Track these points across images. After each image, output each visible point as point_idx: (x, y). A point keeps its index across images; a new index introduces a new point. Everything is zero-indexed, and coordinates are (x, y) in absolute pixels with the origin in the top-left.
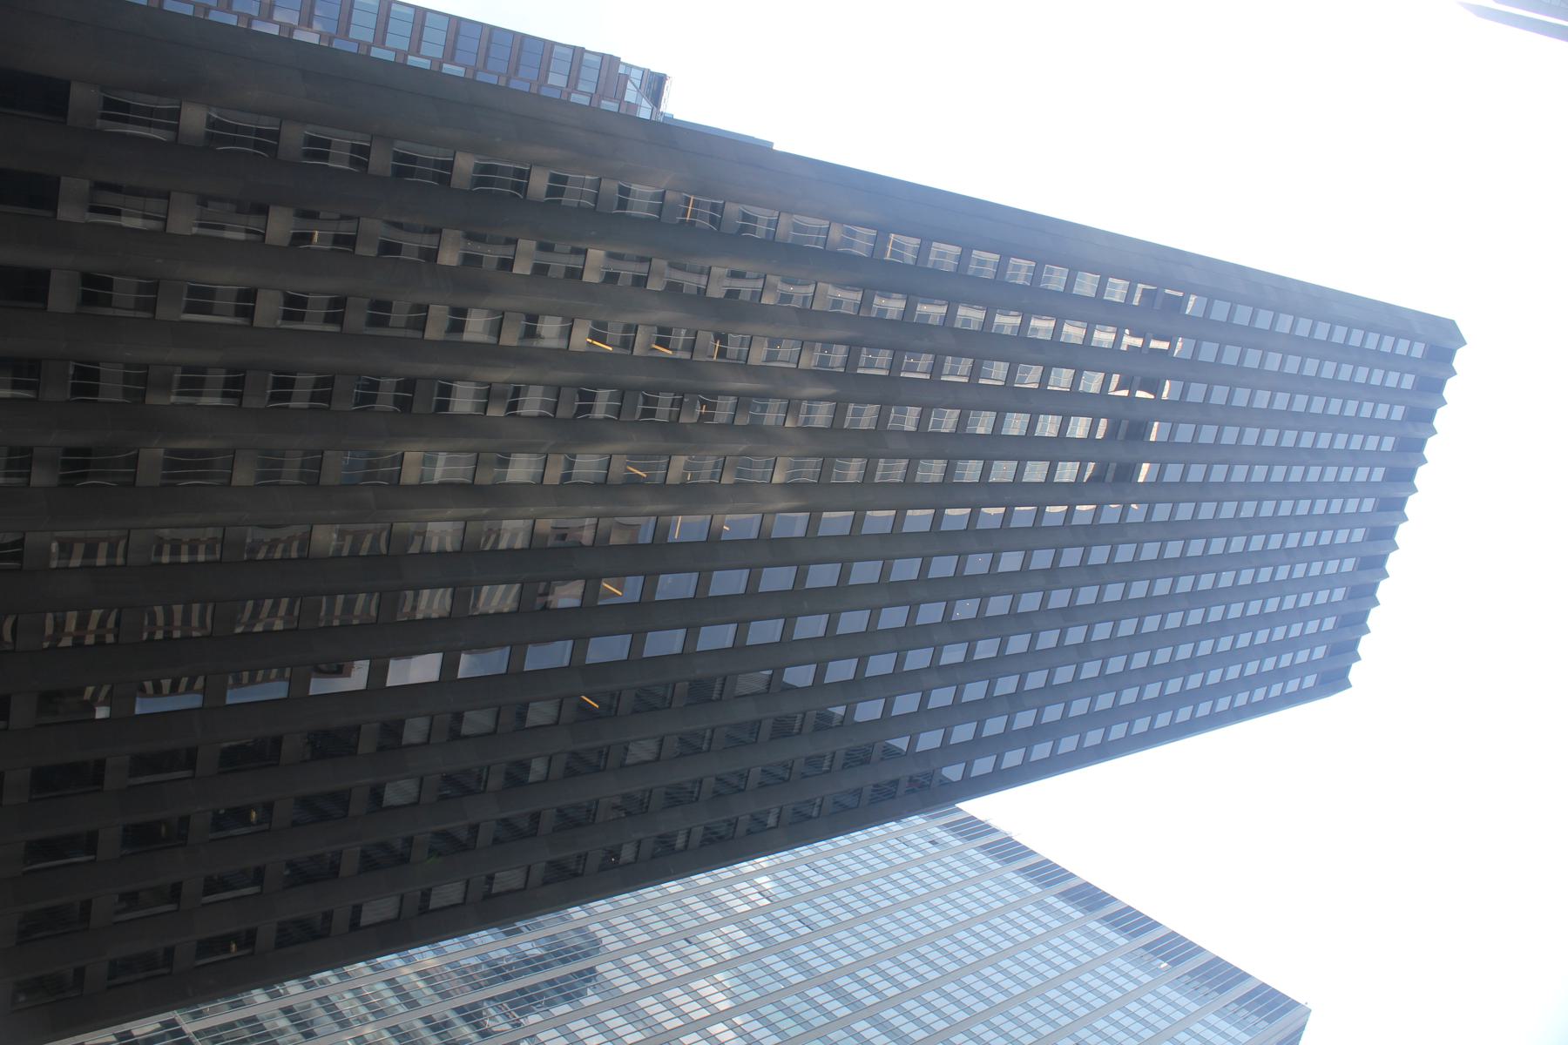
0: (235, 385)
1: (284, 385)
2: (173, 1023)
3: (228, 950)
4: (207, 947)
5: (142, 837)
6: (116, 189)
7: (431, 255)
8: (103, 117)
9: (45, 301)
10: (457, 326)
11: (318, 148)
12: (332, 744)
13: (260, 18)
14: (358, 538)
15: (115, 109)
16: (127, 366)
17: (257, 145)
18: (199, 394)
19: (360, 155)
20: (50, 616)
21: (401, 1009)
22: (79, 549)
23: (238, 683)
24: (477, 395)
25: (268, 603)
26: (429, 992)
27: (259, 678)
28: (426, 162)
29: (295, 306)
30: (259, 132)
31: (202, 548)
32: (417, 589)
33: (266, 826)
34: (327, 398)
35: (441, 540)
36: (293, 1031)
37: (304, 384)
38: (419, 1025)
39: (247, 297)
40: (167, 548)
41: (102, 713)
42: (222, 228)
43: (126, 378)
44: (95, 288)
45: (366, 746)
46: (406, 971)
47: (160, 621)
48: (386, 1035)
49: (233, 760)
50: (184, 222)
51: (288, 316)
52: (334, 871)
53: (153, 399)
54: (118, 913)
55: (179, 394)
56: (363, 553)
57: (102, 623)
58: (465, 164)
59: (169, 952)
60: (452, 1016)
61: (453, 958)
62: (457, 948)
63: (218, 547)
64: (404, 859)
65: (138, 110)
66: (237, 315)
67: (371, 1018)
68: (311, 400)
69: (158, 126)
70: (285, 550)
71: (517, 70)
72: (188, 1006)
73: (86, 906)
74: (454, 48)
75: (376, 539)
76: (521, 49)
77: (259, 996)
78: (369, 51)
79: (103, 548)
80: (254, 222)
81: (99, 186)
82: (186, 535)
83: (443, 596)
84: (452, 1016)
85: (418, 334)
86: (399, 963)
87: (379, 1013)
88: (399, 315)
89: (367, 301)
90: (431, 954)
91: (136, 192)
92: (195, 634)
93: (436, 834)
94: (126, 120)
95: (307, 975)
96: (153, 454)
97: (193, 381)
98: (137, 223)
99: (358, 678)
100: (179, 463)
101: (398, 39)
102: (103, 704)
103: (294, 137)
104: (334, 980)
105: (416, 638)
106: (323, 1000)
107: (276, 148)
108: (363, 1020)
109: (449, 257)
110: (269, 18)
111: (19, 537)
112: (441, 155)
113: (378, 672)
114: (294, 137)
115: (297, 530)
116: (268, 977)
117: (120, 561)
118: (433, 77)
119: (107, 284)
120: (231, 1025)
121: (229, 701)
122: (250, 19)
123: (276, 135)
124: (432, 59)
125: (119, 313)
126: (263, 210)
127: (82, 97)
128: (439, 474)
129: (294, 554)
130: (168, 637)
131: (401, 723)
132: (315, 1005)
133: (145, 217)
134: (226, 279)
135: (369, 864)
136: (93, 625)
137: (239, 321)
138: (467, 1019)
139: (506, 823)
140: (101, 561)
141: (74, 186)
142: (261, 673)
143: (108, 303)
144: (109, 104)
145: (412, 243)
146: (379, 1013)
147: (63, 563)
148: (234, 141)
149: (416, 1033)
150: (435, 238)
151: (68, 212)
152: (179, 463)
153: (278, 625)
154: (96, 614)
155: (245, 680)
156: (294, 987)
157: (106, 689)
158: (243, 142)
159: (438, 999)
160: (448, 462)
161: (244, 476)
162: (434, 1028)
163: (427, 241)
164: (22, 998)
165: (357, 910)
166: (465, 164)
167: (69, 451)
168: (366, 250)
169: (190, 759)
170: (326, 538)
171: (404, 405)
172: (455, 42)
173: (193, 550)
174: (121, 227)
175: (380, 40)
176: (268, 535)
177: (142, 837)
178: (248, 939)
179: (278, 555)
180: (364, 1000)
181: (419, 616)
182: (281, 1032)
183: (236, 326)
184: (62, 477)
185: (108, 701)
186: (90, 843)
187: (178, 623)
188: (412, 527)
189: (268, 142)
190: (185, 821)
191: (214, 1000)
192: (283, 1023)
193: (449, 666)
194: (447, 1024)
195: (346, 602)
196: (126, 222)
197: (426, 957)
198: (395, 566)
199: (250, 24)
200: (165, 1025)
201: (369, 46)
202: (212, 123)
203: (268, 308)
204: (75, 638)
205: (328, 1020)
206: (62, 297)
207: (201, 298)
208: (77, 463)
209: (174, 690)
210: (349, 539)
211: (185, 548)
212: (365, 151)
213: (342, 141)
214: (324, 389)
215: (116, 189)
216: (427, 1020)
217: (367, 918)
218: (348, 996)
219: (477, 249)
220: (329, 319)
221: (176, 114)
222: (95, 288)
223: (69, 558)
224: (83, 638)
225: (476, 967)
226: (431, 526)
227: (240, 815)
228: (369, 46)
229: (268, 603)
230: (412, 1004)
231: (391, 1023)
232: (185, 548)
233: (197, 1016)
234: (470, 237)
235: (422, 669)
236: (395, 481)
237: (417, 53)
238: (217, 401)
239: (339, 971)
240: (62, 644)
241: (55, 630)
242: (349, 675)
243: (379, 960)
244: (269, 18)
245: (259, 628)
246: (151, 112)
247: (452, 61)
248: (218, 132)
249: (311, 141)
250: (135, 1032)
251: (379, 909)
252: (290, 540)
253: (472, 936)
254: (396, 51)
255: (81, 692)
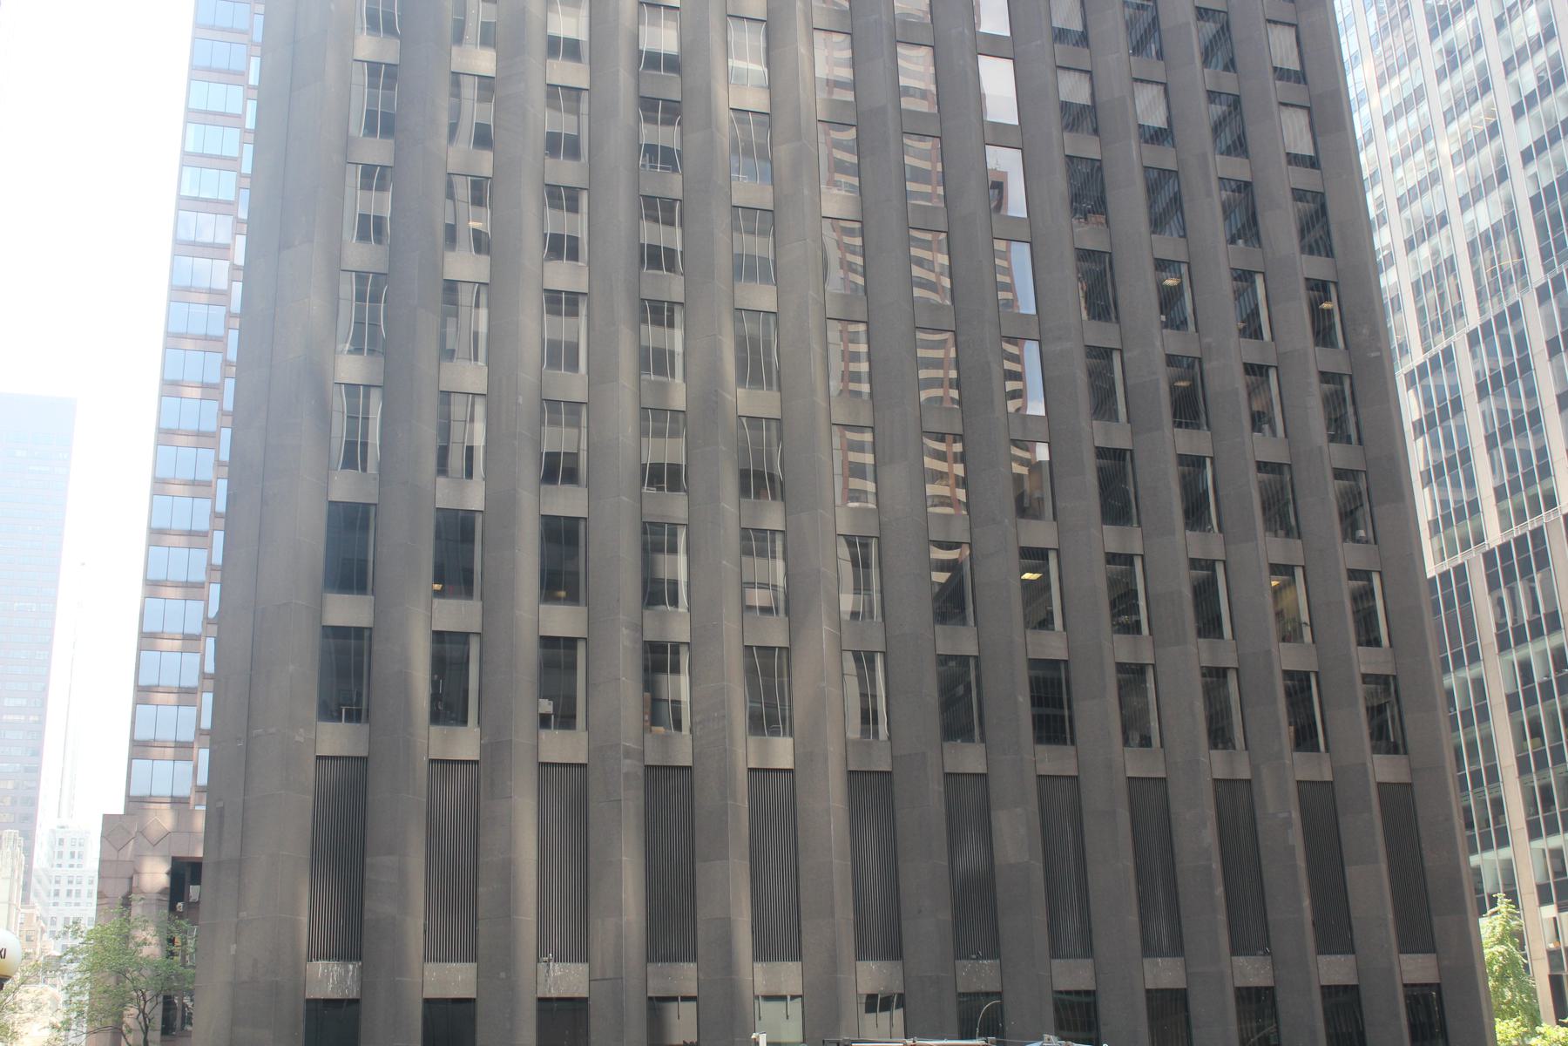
0: (658, 312)
1: (656, 257)
2: (1410, 378)
3: (1330, 312)
4: (1323, 333)
6: (443, 454)
7: (487, 85)
8: (364, 469)
9: (577, 519)
10: (571, 49)
11: (370, 228)
12: (1088, 192)
13: (227, 304)
14: (839, 167)
15: (354, 456)
16: (643, 432)
17: (375, 299)
18: (672, 353)
19: (373, 177)
21: (1424, 107)
22: (855, 483)
23: (1011, 303)
24: (654, 23)
25: (917, 271)
26: (1405, 73)
27: (1007, 280)
28: (372, 99)
29: (561, 247)
30: (360, 297)
32: (900, 92)
33: (1184, 268)
34: (669, 205)
35: (838, 64)
36: (1435, 239)
37: (654, 234)
38: (1446, 85)
39: (560, 302)
40: (852, 386)
41: (1042, 453)
42: (476, 334)
43: (659, 434)
44: (557, 470)
45: (1089, 148)
46: (1375, 102)
47: (938, 392)
48: (1454, 127)
49: (1101, 299)
50: (471, 376)
51: (574, 255)
52: (1245, 187)
53: (678, 400)
55: (673, 376)
56: (855, 159)
57: (941, 456)
58: (367, 47)
59: (1325, 377)
60: (1440, 44)
61: (1366, 43)
62: (1353, 39)
63: (852, 328)
64: (1236, 103)
65: (351, 431)
66: (576, 314)
67: (1431, 145)
68: (673, 224)
70: (854, 253)
71: (235, 73)
72: (1392, 360)
73: (1262, 466)
74: (228, 72)
75: (838, 145)
76: (212, 28)
77: (1388, 280)
78: (246, 176)
79: (854, 457)
80: (466, 296)
81: (442, 468)
82: (837, 365)
83: (907, 59)
84: (1440, 44)
85: (585, 95)
86: (1365, 110)
87: (1425, 136)
88: (564, 124)
89: (549, 161)
90: (1358, 72)
91: (445, 429)
92: (953, 354)
93: (1206, 62)
95: (1369, 223)
96: (747, 401)
97: (656, 361)
98: (479, 428)
99: (1005, 161)
100: (754, 368)
101: (217, 229)
102: (1033, 452)
103: (360, 255)
104: (1378, 190)
105: (957, 88)
106: (1402, 203)
107: (377, 274)
108: (1433, 156)
109: (484, 62)
110: (226, 294)
111: (842, 541)
112: (361, 77)
113: (1001, 135)
114: (360, 255)
115: (830, 237)
116: (1366, 268)
118: (265, 96)
119: (552, 458)
120: (1421, 311)
121: (1033, 311)
122: (229, 315)
123: (361, 277)
124: (246, 98)
125: (584, 445)
126: (451, 287)
127: (345, 487)
128: (758, 69)
129: (858, 241)
130: (957, 384)
131: (1065, 106)
132: (1407, 213)
133: (472, 420)
134: (532, 327)
135: (1239, 147)
137: (583, 310)
138: (1446, 23)
139: (1207, 56)
140: (868, 459)
141: (447, 494)
142: (1000, 278)
144: (349, 462)
145: (474, 112)
146: (1425, 136)
147: (871, 498)
148: (374, 325)
149: (1455, 91)
150: (465, 80)
151: (474, 498)
152: (754, 368)
154: (930, 463)
155: (1009, 296)
156: (1382, 239)
157: (1016, 451)
159: (1416, 62)
160: (741, 57)
161: (763, 297)
162: (1453, 66)
163: (470, 90)
164: (1362, 533)
165: (1294, 159)
166: (367, 47)
167: (744, 491)
168: (485, 163)
169: (1100, 355)
170: (836, 201)
171: (672, 112)
172: (219, 71)
173: (855, 357)
174: (486, 447)
175: (231, 163)
176: (836, 274)
178: (1319, 288)
179: (859, 260)
180: (1406, 155)
181: (933, 88)
182: (1435, 253)
183: (588, 316)
184: (774, 498)
186: (1192, 464)
187: (940, 373)
188: (822, 95)
189: (371, 288)
190: (1171, 360)
191: (1387, 331)
192: (1424, 251)
193: (994, 47)
194: (1450, 51)
195: (916, 181)
196: (479, 441)
197: (1359, 78)
198: (869, 119)
200: (1411, 383)
201: (241, 176)
203: (563, 276)
205: (1427, 197)
206: (567, 502)
207: (560, 355)
210: (838, 177)
211: (853, 367)
212: (368, 171)
213: (359, 201)
214: (658, 209)
215: (443, 454)
216: (1441, 75)
217: (1305, 148)
218: (1399, 173)
219: (473, 30)
220: (574, 208)
221: (352, 388)
222: (557, 470)
223: (865, 492)
224: (957, 476)
225: (1380, 14)
226: (822, 71)
227: (1169, 300)
228: (241, 176)
229: (917, 271)
230: (1419, 95)
231: (1439, 120)
232: (853, 367)
233: (1404, 349)
234: (459, 38)
235: (998, 83)
236: (767, 119)
237: (241, 117)
238: (678, 334)
239: (1367, 185)
240: (964, 499)
242: (1005, 174)
243: (1359, 135)
244: (226, 294)
245: (946, 282)
246: (352, 418)
247: (243, 74)
248: (366, 340)
249: (363, 236)
250: (1416, 417)
251: (1295, 133)
252: (840, 244)
253: (1339, 19)
254: (242, 143)
255: (1018, 478)
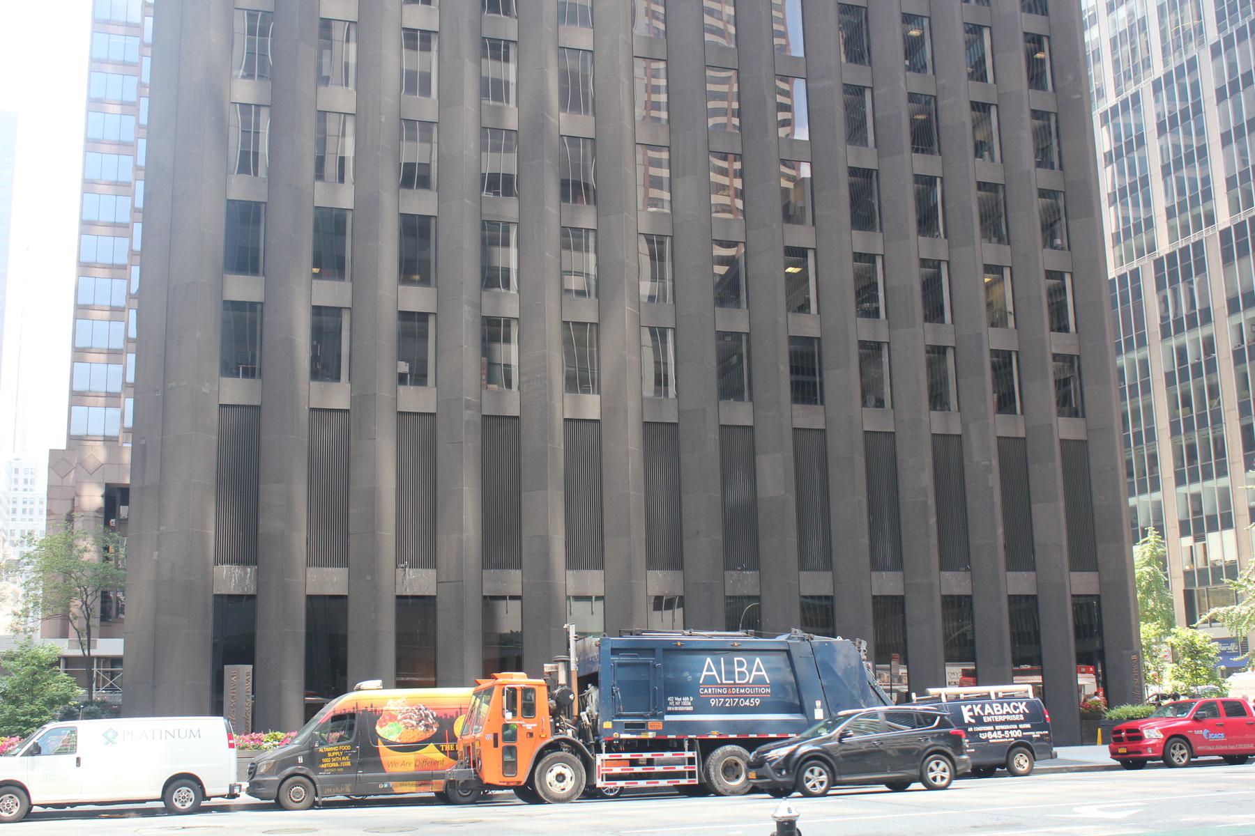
0: (496, 49)
3: (1042, 61)
4: (1036, 79)
5: (924, 137)
8: (256, 174)
9: (429, 217)
13: (141, 36)
17: (264, 33)
18: (507, 83)
20: (714, 215)
22: (654, 193)
23: (784, 48)
25: (708, 20)
27: (781, 28)
30: (251, 32)
31: (654, 82)
33: (926, 22)
39: (416, 39)
40: (654, 113)
41: (805, 171)
42: (347, 65)
44: (413, 177)
50: (342, 99)
53: (512, 122)
54: (992, 159)
55: (508, 101)
57: (723, 172)
59: (1036, 114)
63: (654, 65)
65: (245, 143)
66: (429, 50)
69: (257, 125)
72: (1090, 102)
77: (1091, 36)
79: (654, 171)
80: (338, 33)
81: (320, 174)
82: (641, 97)
91: (322, 143)
92: (735, 89)
94: (256, 154)
96: (568, 123)
97: (494, 90)
98: (350, 142)
100: (573, 97)
111: (642, 239)
117: (665, 155)
119: (410, 167)
120: (1116, 63)
121: (801, 54)
123: (252, 15)
125: (435, 157)
126: (326, 24)
127: (240, 188)
133: (344, 135)
136: (725, 181)
140: (665, 173)
142: (776, 27)
143: (427, 166)
147: (667, 205)
148: (263, 55)
151: (345, 198)
152: (573, 97)
153: (730, 10)
154: (715, 178)
155: (783, 42)
157: (784, 169)
158: (263, 47)
161: (582, 38)
164: (1058, 241)
167: (564, 196)
169: (855, 92)
173: (656, 89)
176: (642, 20)
177: (924, 137)
178: (1035, 41)
182: (1131, 14)
183: (439, 51)
184: (588, 202)
185: (791, 163)
186: (925, 182)
187: (724, 104)
190: (912, 97)
191: (1088, 78)
192: (1122, 12)
196: (349, 153)
199: (147, 45)
200: (1104, 121)
202: (249, 75)
204: (735, 177)
206: (421, 203)
207: (416, 83)
208: (574, 189)
209: (787, 108)
211: (654, 98)
221: (245, 107)
222: (413, 177)
227: (912, 48)
229: (708, 20)
232: (654, 98)
233: (1101, 93)
238: (512, 67)
241: (730, 212)
245: (732, 30)
246: (246, 132)
248: (256, 67)
250: (1107, 149)
255: (785, 191)
